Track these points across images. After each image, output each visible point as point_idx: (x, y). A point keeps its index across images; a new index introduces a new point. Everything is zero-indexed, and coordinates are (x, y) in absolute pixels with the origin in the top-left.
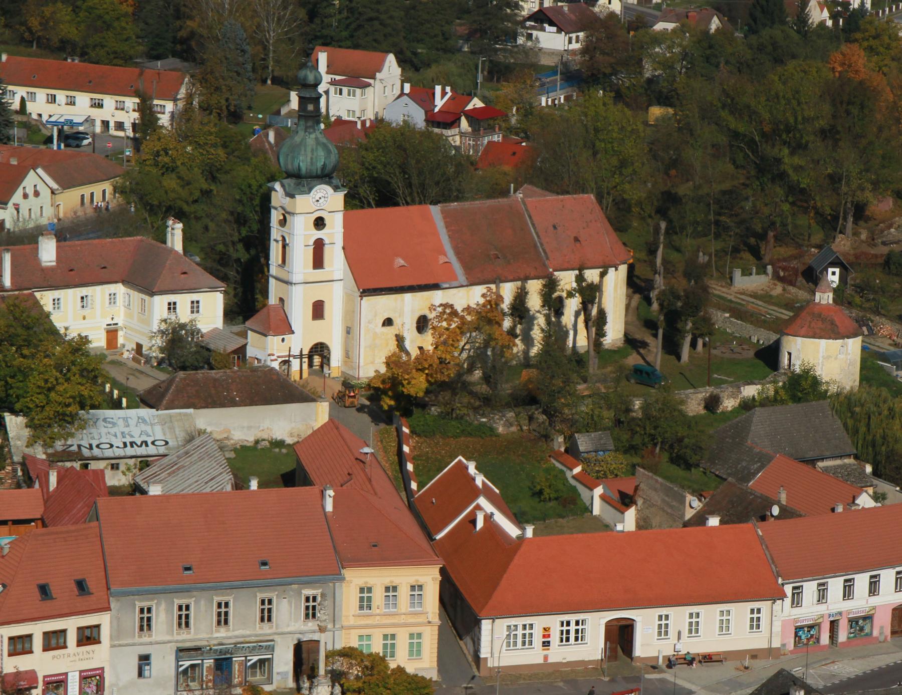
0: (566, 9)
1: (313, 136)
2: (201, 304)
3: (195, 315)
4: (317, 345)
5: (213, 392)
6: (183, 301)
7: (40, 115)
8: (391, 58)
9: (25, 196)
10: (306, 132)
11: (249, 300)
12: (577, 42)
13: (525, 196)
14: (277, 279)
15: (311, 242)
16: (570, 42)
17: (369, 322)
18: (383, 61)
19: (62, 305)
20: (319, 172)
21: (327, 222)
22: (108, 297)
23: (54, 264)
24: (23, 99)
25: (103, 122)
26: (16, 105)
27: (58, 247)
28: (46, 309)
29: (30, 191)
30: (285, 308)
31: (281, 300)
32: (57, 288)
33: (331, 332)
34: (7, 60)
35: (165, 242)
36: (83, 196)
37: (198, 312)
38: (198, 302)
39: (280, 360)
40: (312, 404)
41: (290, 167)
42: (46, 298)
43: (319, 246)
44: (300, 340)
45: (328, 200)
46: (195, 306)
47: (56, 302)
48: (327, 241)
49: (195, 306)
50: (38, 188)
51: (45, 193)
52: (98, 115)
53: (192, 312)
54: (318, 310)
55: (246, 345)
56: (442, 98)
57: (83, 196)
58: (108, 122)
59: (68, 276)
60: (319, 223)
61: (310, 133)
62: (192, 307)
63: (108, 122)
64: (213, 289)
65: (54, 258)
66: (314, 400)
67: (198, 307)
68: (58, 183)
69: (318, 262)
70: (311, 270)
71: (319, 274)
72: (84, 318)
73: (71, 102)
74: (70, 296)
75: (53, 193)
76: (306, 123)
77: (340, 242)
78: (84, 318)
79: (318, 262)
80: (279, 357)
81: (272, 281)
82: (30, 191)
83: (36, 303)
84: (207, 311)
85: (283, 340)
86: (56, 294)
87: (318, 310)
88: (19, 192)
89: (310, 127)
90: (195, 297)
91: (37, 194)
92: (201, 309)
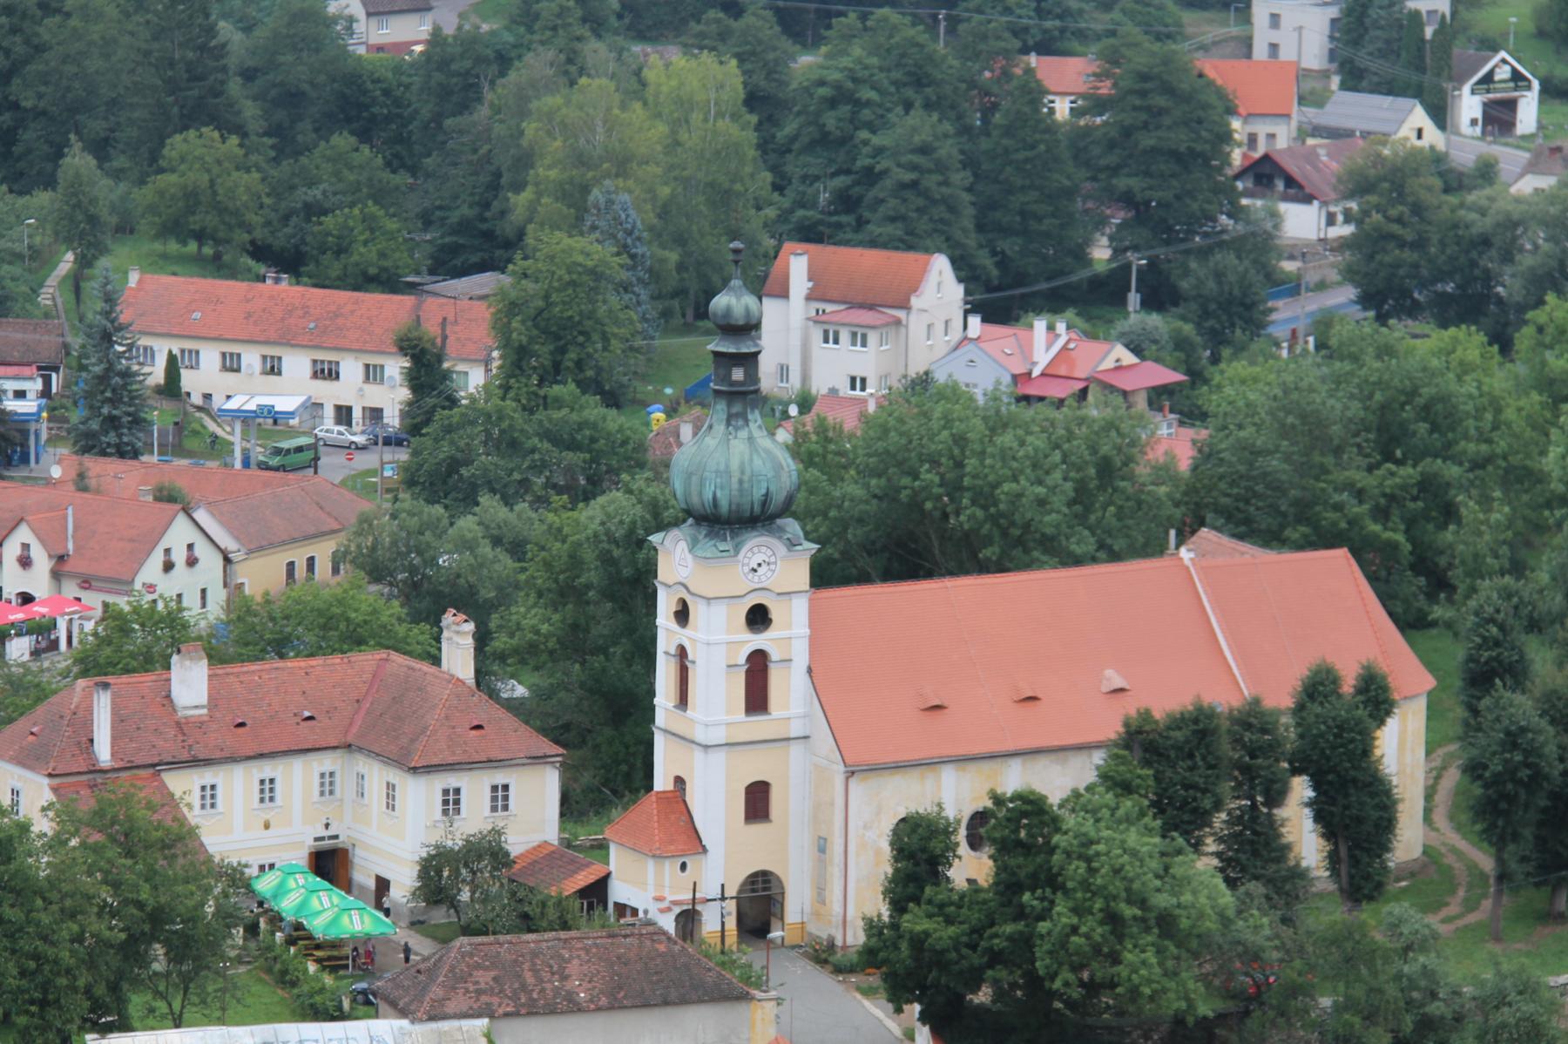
0: (1322, 152)
1: (743, 434)
2: (512, 792)
3: (500, 819)
4: (755, 875)
5: (529, 978)
6: (475, 788)
7: (207, 397)
8: (941, 265)
9: (168, 566)
10: (728, 423)
11: (608, 751)
12: (1347, 221)
13: (1202, 554)
14: (665, 731)
15: (742, 659)
16: (1331, 220)
17: (865, 827)
18: (924, 270)
19: (219, 800)
20: (757, 509)
21: (774, 614)
22: (317, 780)
23: (205, 711)
24: (172, 359)
25: (338, 408)
26: (156, 373)
27: (210, 677)
28: (926, 1029)
29: (179, 557)
30: (688, 799)
31: (679, 781)
32: (207, 762)
33: (784, 848)
34: (140, 282)
35: (436, 660)
36: (291, 565)
37: (506, 808)
38: (506, 787)
39: (677, 910)
40: (741, 1009)
41: (695, 500)
42: (184, 785)
43: (758, 665)
44: (719, 872)
45: (778, 566)
46: (500, 798)
47: (209, 795)
48: (774, 655)
49: (500, 798)
50: (197, 552)
51: (210, 562)
52: (330, 394)
53: (494, 809)
54: (757, 801)
55: (608, 875)
56: (1049, 346)
57: (291, 565)
58: (349, 409)
59: (237, 740)
60: (758, 617)
61: (737, 429)
62: (494, 799)
63: (349, 409)
64: (538, 759)
65: (204, 700)
66: (744, 997)
67: (506, 798)
68: (237, 538)
69: (757, 700)
70: (740, 715)
71: (759, 726)
72: (267, 826)
73: (273, 368)
74: (237, 783)
75: (227, 560)
76: (729, 406)
77: (801, 658)
78: (267, 826)
79: (757, 700)
80: (675, 903)
81: (659, 742)
82: (179, 557)
83: (170, 800)
84: (530, 809)
85: (683, 867)
86: (207, 776)
87: (757, 801)
88: (157, 558)
89: (737, 415)
90: (500, 778)
91: (192, 562)
92: (511, 802)
